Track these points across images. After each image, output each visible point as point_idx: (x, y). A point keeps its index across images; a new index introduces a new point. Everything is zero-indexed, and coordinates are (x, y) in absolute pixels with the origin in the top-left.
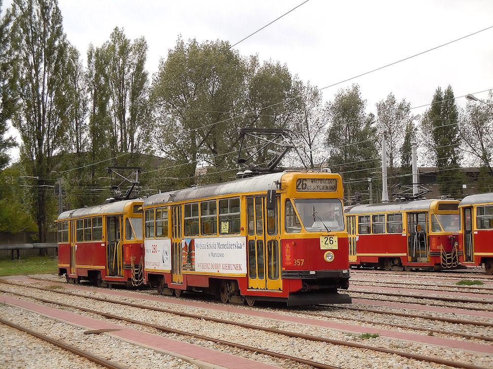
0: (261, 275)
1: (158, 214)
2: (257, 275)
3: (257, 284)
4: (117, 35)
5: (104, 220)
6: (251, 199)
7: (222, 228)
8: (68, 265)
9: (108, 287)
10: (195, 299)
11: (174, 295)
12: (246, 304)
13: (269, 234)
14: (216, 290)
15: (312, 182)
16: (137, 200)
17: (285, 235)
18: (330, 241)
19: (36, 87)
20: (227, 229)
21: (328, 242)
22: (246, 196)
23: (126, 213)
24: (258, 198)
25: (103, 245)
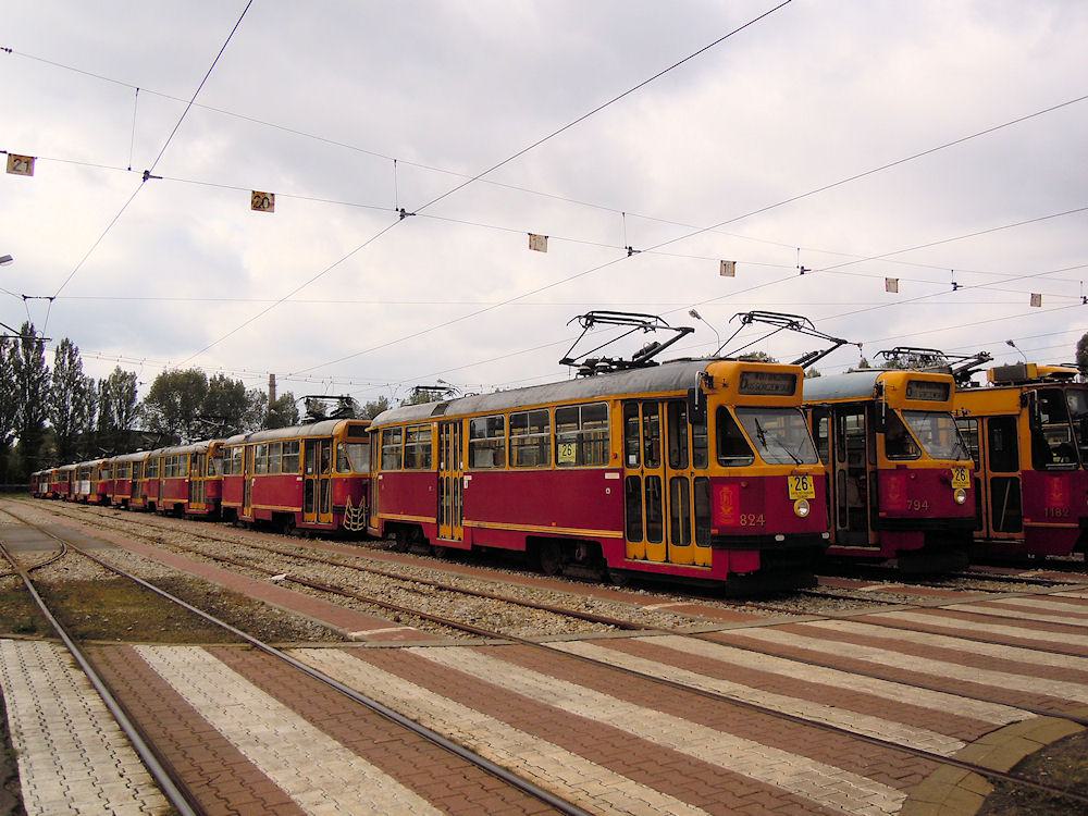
0: (655, 536)
1: (408, 434)
2: (645, 535)
3: (311, 519)
4: (118, 370)
5: (302, 445)
6: (135, 463)
7: (560, 455)
8: (240, 505)
9: (191, 520)
10: (521, 570)
11: (246, 527)
12: (434, 556)
13: (840, 461)
14: (85, 501)
15: (757, 377)
16: (220, 441)
17: (715, 469)
18: (803, 483)
19: (64, 401)
20: (574, 454)
21: (800, 487)
22: (622, 400)
23: (337, 436)
24: (650, 406)
25: (300, 479)
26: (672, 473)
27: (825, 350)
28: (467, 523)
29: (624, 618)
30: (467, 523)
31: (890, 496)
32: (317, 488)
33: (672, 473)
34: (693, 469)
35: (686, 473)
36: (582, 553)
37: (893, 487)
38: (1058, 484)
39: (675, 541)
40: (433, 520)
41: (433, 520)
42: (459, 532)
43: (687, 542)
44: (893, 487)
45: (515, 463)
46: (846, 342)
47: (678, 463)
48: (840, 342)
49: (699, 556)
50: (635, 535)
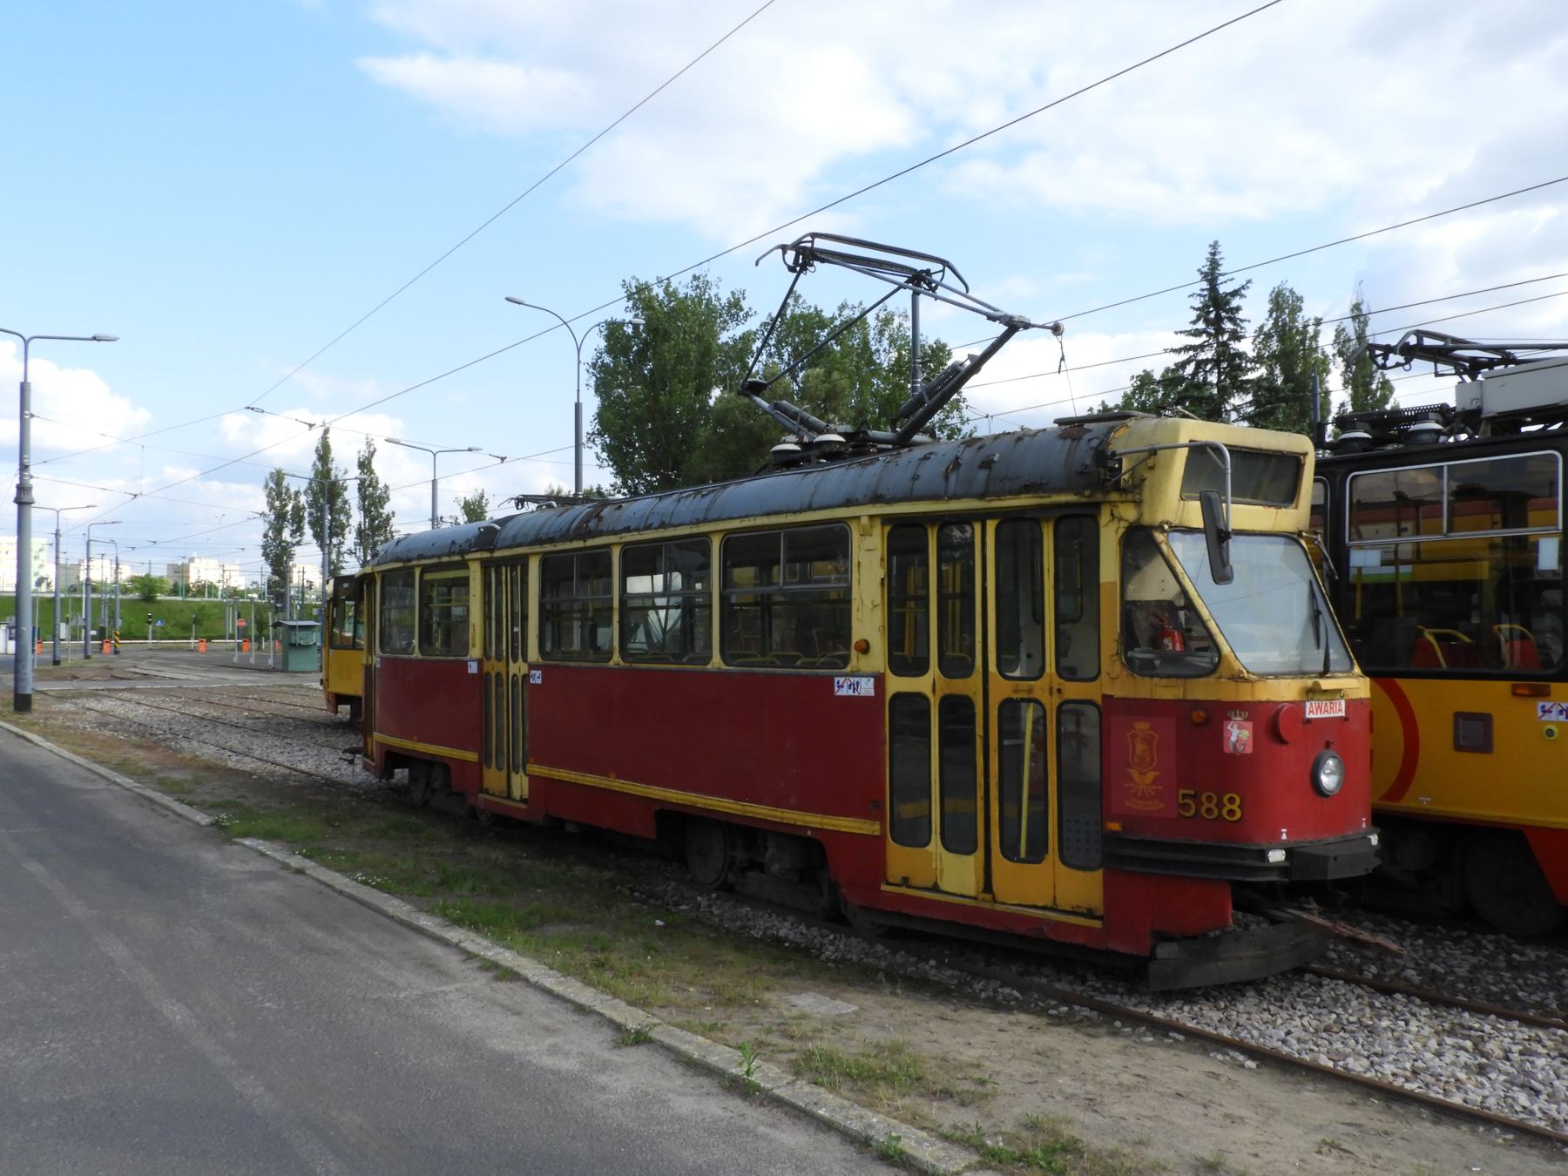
0: (958, 842)
26: (971, 686)
27: (978, 352)
28: (536, 769)
29: (582, 1000)
30: (536, 769)
31: (1135, 773)
32: (987, 728)
33: (1001, 689)
34: (1057, 682)
35: (1039, 689)
36: (778, 861)
37: (1140, 747)
38: (1148, 741)
39: (1010, 852)
40: (472, 756)
41: (472, 756)
42: (520, 785)
43: (1037, 853)
44: (1140, 747)
45: (428, 577)
46: (1027, 326)
47: (956, 666)
48: (1013, 326)
49: (1055, 888)
50: (914, 835)
